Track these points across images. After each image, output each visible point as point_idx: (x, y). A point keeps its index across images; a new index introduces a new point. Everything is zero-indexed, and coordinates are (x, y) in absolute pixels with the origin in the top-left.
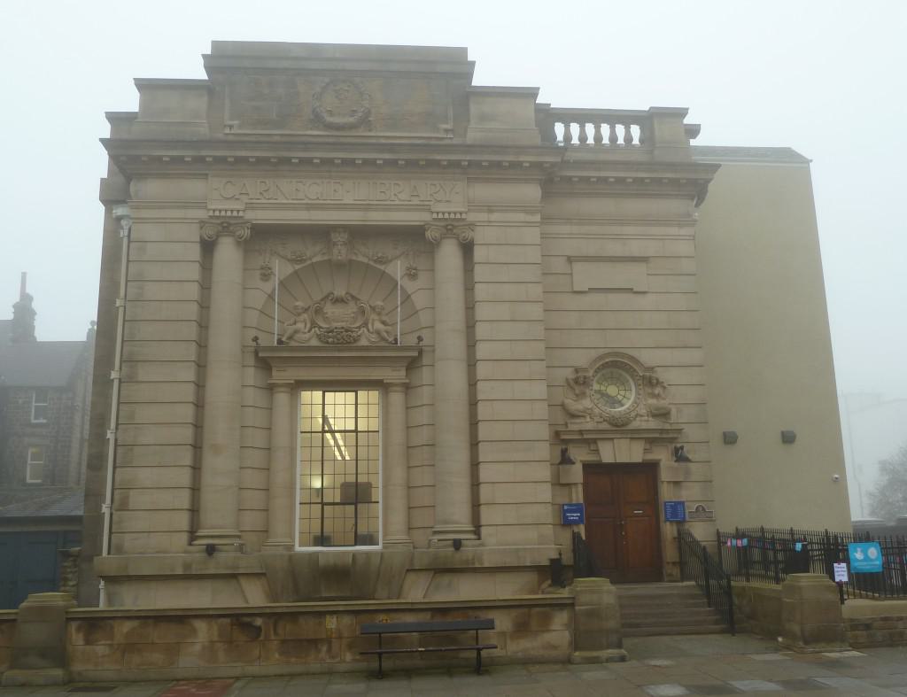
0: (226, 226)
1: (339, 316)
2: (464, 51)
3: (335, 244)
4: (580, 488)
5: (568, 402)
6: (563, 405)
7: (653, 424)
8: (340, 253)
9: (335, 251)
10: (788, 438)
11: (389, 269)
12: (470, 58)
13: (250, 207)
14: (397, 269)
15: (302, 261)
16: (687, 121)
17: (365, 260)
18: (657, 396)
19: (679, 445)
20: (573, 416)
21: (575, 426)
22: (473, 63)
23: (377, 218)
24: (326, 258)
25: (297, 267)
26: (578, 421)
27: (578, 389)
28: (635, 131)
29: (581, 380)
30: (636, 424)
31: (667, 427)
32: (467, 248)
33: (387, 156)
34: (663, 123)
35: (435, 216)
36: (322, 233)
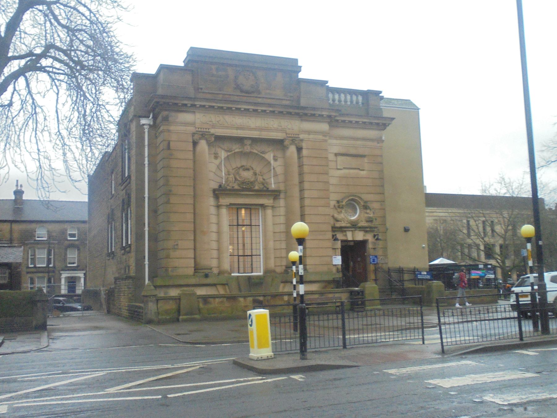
0: (203, 135)
1: (247, 175)
2: (296, 60)
3: (246, 145)
4: (340, 250)
5: (336, 215)
6: (333, 216)
7: (366, 224)
8: (247, 149)
9: (245, 148)
10: (406, 230)
11: (266, 156)
12: (299, 65)
13: (214, 126)
14: (270, 156)
15: (231, 151)
16: (381, 95)
17: (256, 152)
18: (367, 213)
19: (376, 234)
20: (337, 221)
21: (338, 225)
22: (301, 67)
23: (265, 135)
24: (241, 150)
25: (229, 154)
26: (339, 223)
27: (339, 210)
28: (360, 98)
29: (341, 206)
30: (359, 225)
31: (373, 226)
32: (299, 149)
33: (271, 109)
34: (371, 97)
35: (197, 129)
36: (240, 140)
